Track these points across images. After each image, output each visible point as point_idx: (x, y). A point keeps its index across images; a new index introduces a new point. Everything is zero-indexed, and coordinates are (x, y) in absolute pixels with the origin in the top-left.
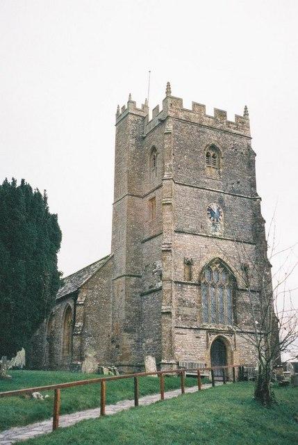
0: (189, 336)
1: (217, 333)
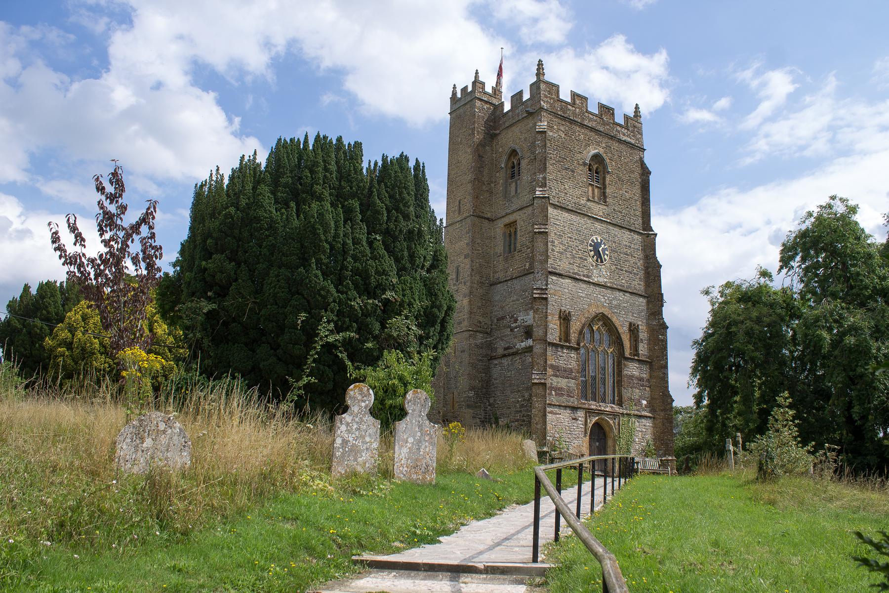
0: (565, 416)
1: (598, 414)
